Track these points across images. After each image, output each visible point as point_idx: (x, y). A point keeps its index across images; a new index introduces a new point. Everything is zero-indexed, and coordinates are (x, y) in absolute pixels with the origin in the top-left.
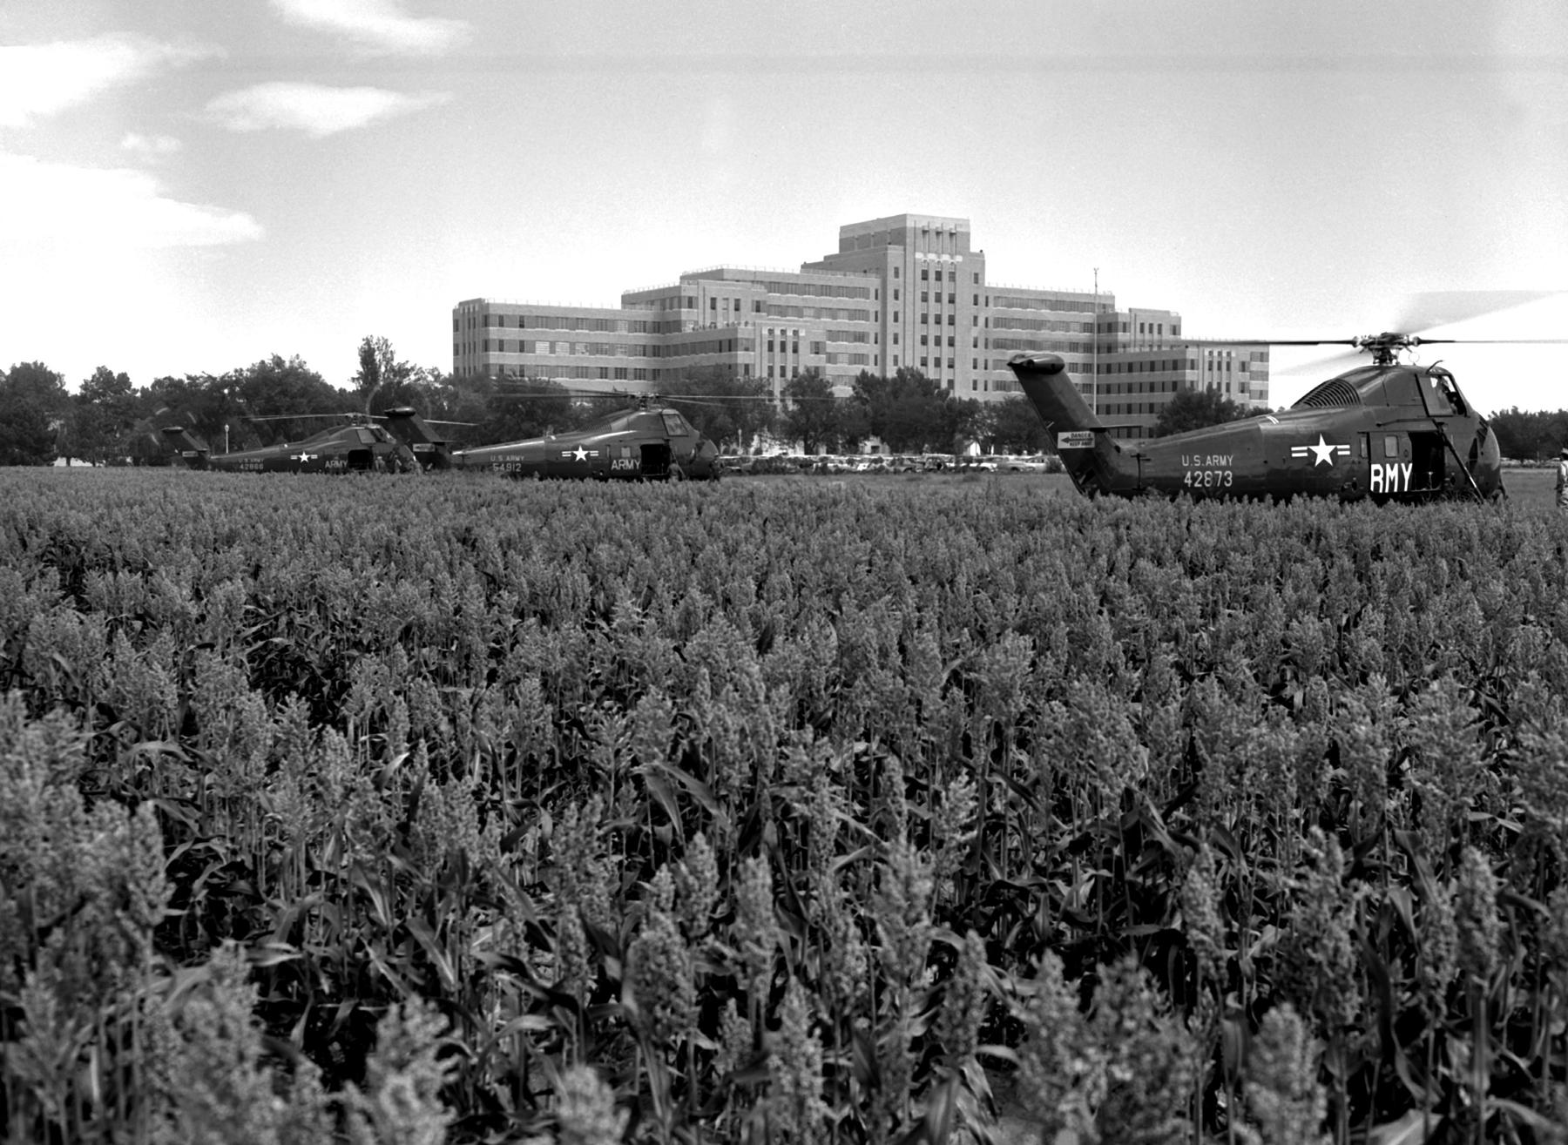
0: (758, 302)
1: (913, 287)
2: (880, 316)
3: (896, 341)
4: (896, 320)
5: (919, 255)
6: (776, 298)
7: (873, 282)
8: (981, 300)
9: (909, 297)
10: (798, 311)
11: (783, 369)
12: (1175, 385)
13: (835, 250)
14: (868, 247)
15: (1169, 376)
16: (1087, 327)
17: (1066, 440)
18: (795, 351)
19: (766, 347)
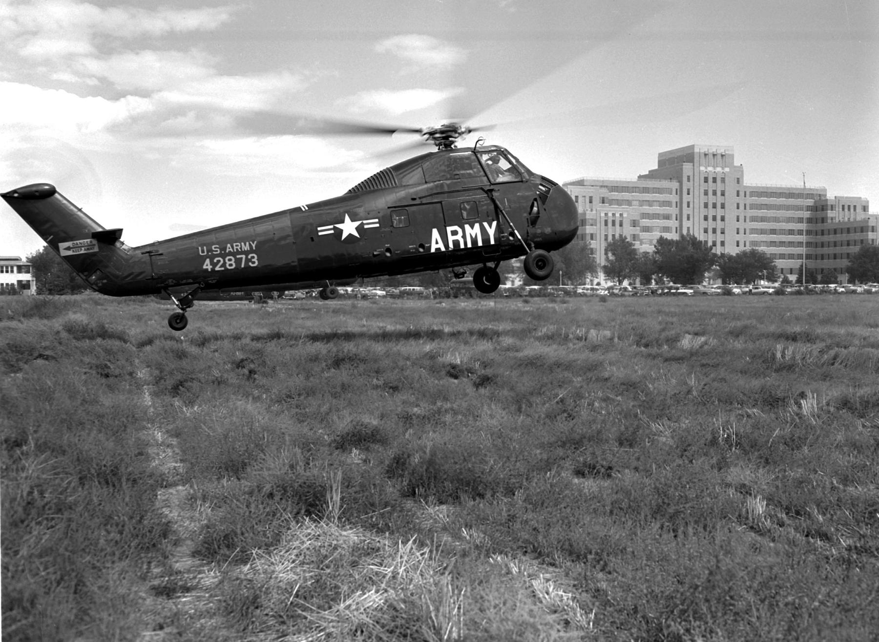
0: (603, 198)
1: (698, 188)
2: (679, 205)
3: (688, 219)
4: (688, 206)
5: (702, 168)
6: (615, 195)
7: (675, 185)
8: (742, 194)
9: (696, 193)
10: (629, 203)
11: (606, 236)
12: (862, 241)
13: (656, 167)
14: (673, 165)
15: (857, 236)
16: (809, 208)
17: (68, 249)
18: (621, 225)
19: (603, 223)
